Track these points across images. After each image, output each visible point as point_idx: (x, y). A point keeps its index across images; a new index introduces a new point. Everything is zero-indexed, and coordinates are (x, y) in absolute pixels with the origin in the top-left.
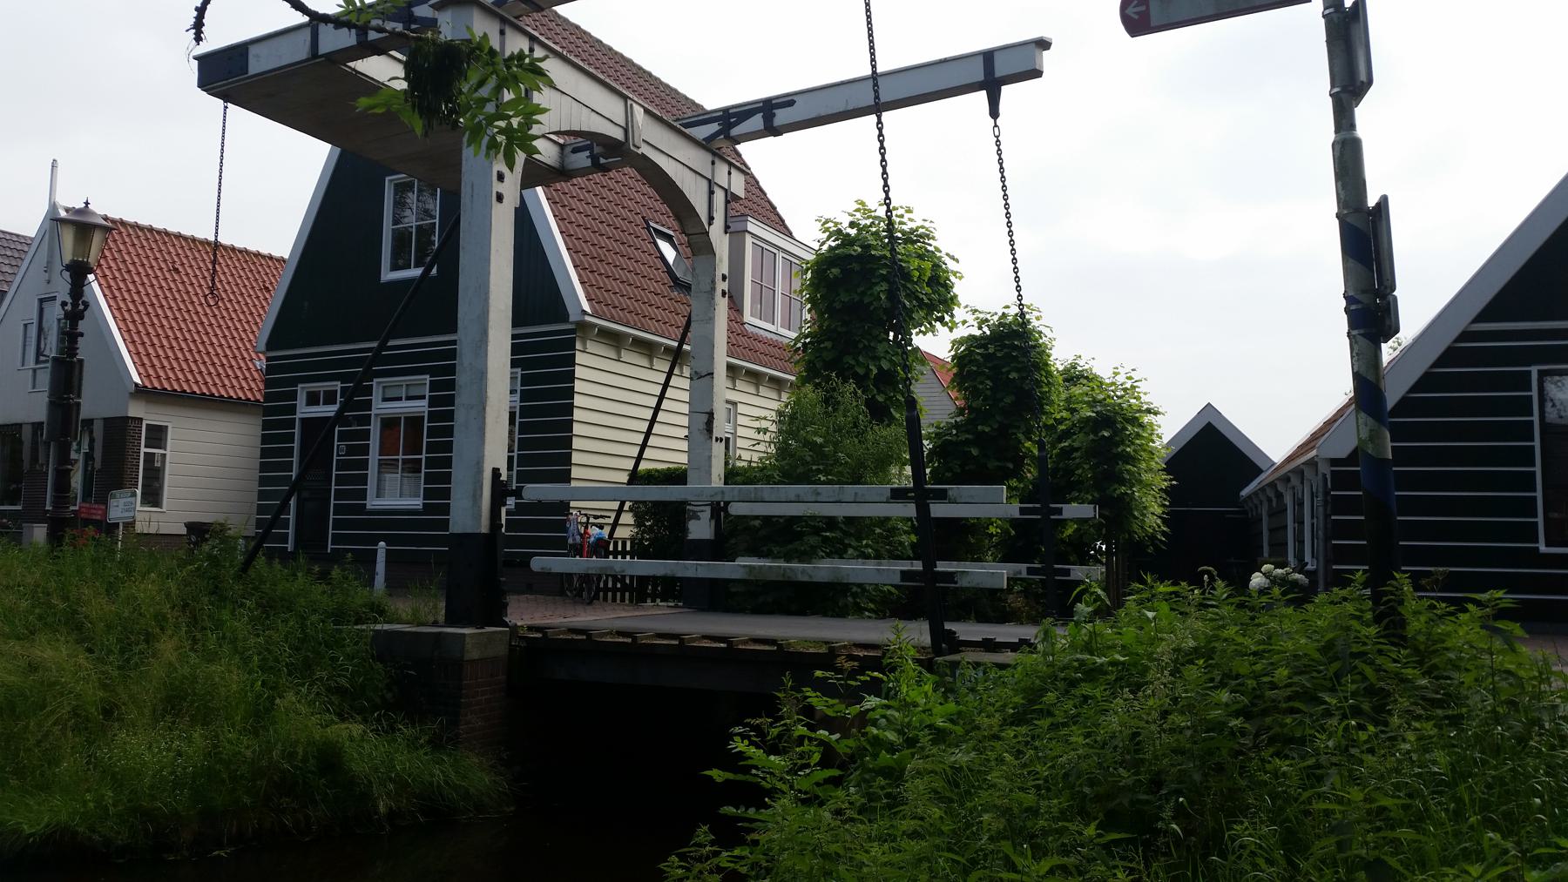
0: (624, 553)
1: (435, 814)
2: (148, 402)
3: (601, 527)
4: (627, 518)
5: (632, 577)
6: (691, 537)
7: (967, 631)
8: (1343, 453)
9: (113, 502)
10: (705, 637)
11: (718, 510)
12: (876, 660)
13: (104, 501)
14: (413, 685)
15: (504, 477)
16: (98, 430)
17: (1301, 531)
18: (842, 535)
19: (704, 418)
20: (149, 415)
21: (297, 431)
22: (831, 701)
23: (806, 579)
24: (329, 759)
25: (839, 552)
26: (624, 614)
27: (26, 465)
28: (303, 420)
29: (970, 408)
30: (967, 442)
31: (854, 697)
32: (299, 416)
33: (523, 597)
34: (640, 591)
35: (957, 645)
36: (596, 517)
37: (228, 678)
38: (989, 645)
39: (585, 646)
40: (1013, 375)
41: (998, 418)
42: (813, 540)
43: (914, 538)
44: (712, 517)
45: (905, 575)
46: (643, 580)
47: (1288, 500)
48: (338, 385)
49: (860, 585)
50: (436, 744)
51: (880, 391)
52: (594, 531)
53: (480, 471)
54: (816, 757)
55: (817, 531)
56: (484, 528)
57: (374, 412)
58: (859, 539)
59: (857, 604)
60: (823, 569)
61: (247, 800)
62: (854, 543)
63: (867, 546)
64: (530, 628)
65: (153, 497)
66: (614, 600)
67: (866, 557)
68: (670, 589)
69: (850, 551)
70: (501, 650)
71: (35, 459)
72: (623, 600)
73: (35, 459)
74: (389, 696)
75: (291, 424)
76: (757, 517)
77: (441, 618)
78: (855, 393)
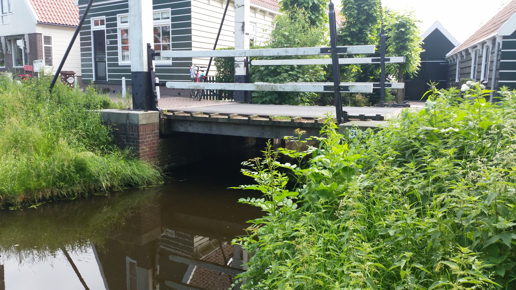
0: (213, 81)
1: (130, 186)
2: (43, 27)
3: (203, 71)
4: (213, 68)
5: (216, 90)
6: (237, 74)
7: (350, 110)
8: (509, 33)
9: (35, 64)
10: (239, 115)
11: (247, 63)
12: (314, 128)
13: (32, 64)
14: (120, 136)
15: (153, 47)
16: (27, 38)
17: (491, 66)
18: (296, 73)
19: (241, 25)
20: (45, 32)
21: (92, 36)
22: (292, 151)
23: (282, 90)
24: (81, 167)
25: (296, 79)
26: (216, 104)
27: (4, 52)
28: (94, 32)
29: (348, 22)
30: (345, 36)
31: (304, 148)
32: (92, 30)
33: (175, 98)
34: (220, 95)
35: (348, 118)
36: (201, 67)
37: (36, 132)
38: (363, 118)
39: (190, 119)
40: (366, 8)
41: (359, 25)
42: (285, 75)
43: (325, 72)
44: (245, 66)
45: (326, 88)
46: (221, 91)
47: (473, 56)
48: (104, 18)
49: (303, 93)
50: (128, 158)
51: (313, 14)
52: (200, 73)
53: (141, 45)
54: (285, 183)
55: (287, 71)
56: (145, 69)
57: (118, 28)
58: (303, 74)
59: (302, 100)
60: (288, 86)
61: (44, 184)
62: (301, 76)
63: (307, 77)
64: (168, 111)
65: (49, 62)
66: (210, 99)
67: (305, 81)
68: (230, 95)
69: (300, 79)
70: (156, 120)
71: (7, 50)
72: (213, 99)
73: (7, 50)
74: (110, 139)
75: (89, 33)
76: (263, 66)
77: (132, 107)
78: (304, 13)
